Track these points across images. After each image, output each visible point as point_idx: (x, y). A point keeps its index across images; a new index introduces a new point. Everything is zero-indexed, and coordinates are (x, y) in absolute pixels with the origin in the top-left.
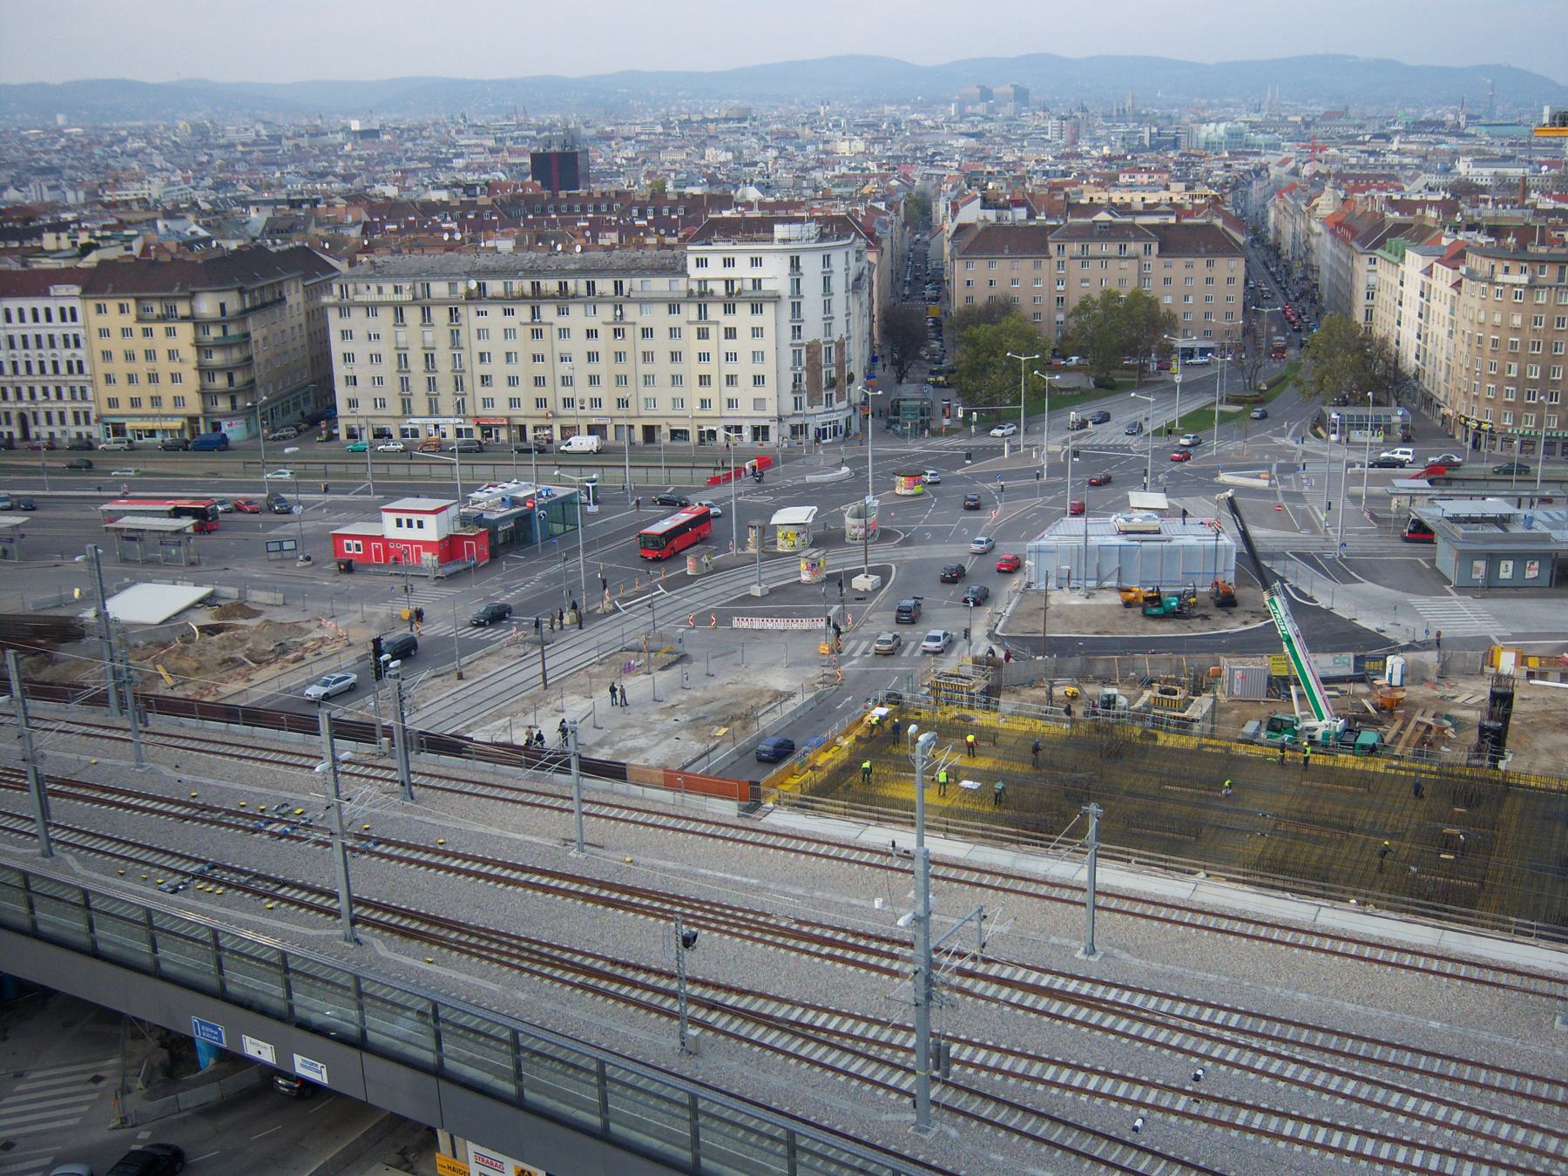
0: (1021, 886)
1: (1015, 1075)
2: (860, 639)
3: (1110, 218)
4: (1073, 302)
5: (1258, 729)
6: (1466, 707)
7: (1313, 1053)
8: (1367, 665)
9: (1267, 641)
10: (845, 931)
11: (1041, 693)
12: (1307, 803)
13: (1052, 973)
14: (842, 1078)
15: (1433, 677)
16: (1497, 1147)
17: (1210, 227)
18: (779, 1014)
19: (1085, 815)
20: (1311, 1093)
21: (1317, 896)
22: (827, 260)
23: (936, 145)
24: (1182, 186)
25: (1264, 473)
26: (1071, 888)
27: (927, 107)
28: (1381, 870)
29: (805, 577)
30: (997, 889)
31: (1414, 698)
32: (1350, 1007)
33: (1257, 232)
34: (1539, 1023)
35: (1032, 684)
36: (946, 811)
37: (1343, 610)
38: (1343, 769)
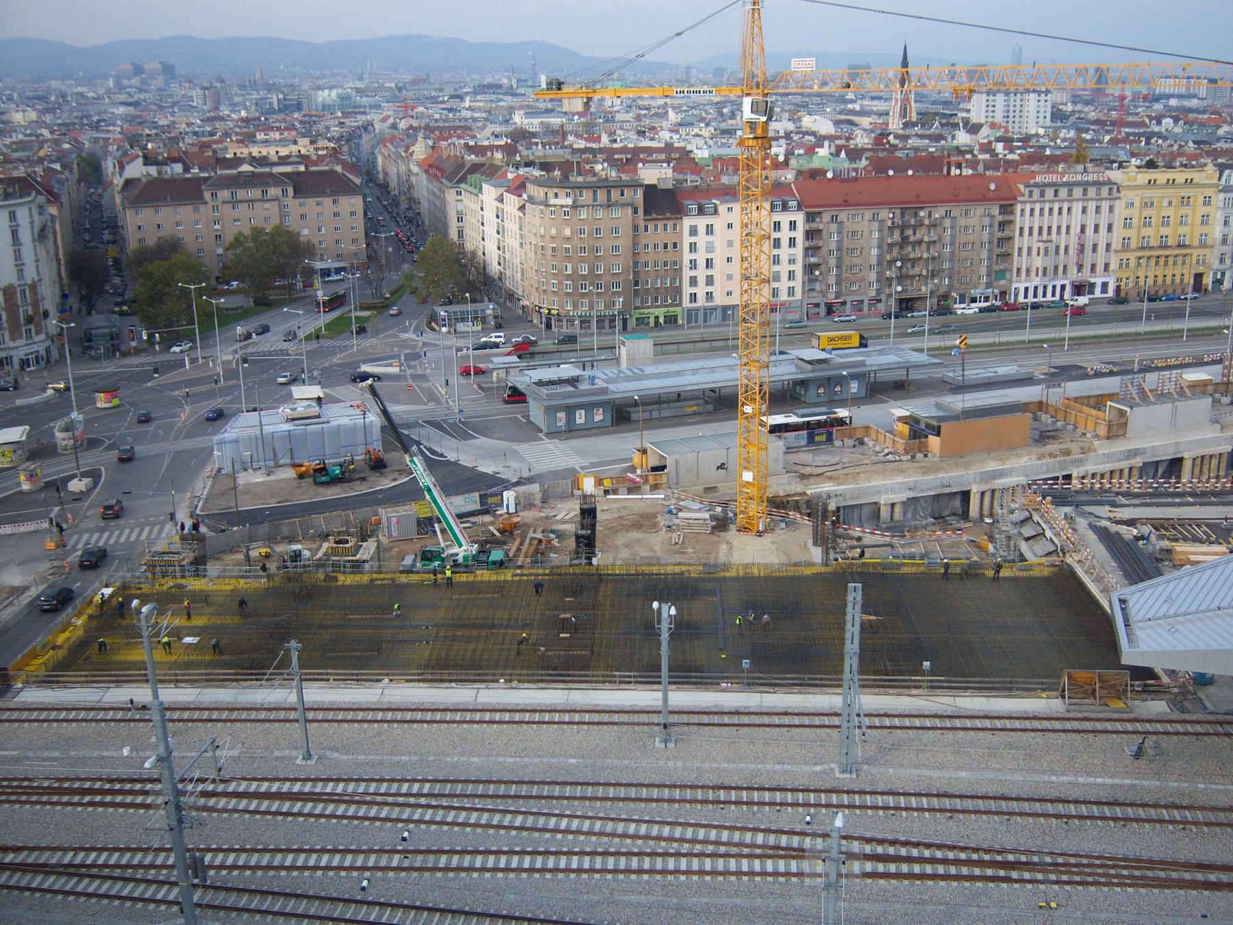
0: (244, 715)
1: (262, 868)
2: (82, 532)
3: (251, 169)
4: (229, 238)
5: (414, 561)
6: (566, 522)
7: (489, 801)
8: (490, 500)
9: (413, 492)
10: (101, 780)
11: (240, 557)
12: (459, 612)
13: (280, 780)
14: (117, 903)
15: (538, 502)
16: (629, 841)
17: (332, 173)
18: (53, 861)
19: (288, 651)
20: (491, 831)
21: (475, 681)
22: (13, 216)
23: (100, 113)
24: (306, 141)
25: (395, 361)
26: (284, 709)
27: (89, 81)
28: (519, 654)
29: (26, 487)
30: (225, 721)
31: (529, 520)
32: (511, 760)
33: (370, 175)
34: (645, 746)
35: (232, 550)
36: (174, 665)
37: (466, 461)
38: (482, 582)
